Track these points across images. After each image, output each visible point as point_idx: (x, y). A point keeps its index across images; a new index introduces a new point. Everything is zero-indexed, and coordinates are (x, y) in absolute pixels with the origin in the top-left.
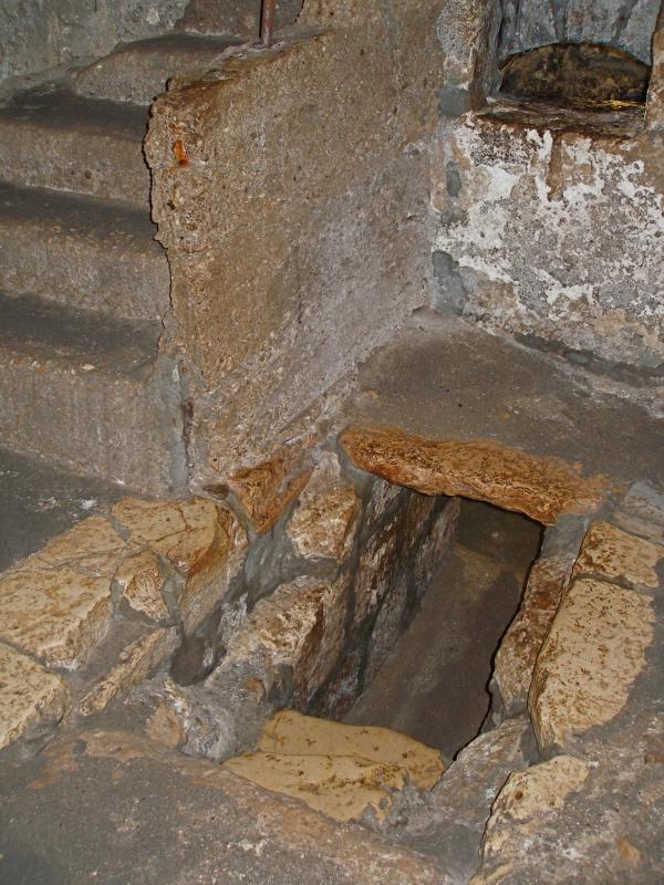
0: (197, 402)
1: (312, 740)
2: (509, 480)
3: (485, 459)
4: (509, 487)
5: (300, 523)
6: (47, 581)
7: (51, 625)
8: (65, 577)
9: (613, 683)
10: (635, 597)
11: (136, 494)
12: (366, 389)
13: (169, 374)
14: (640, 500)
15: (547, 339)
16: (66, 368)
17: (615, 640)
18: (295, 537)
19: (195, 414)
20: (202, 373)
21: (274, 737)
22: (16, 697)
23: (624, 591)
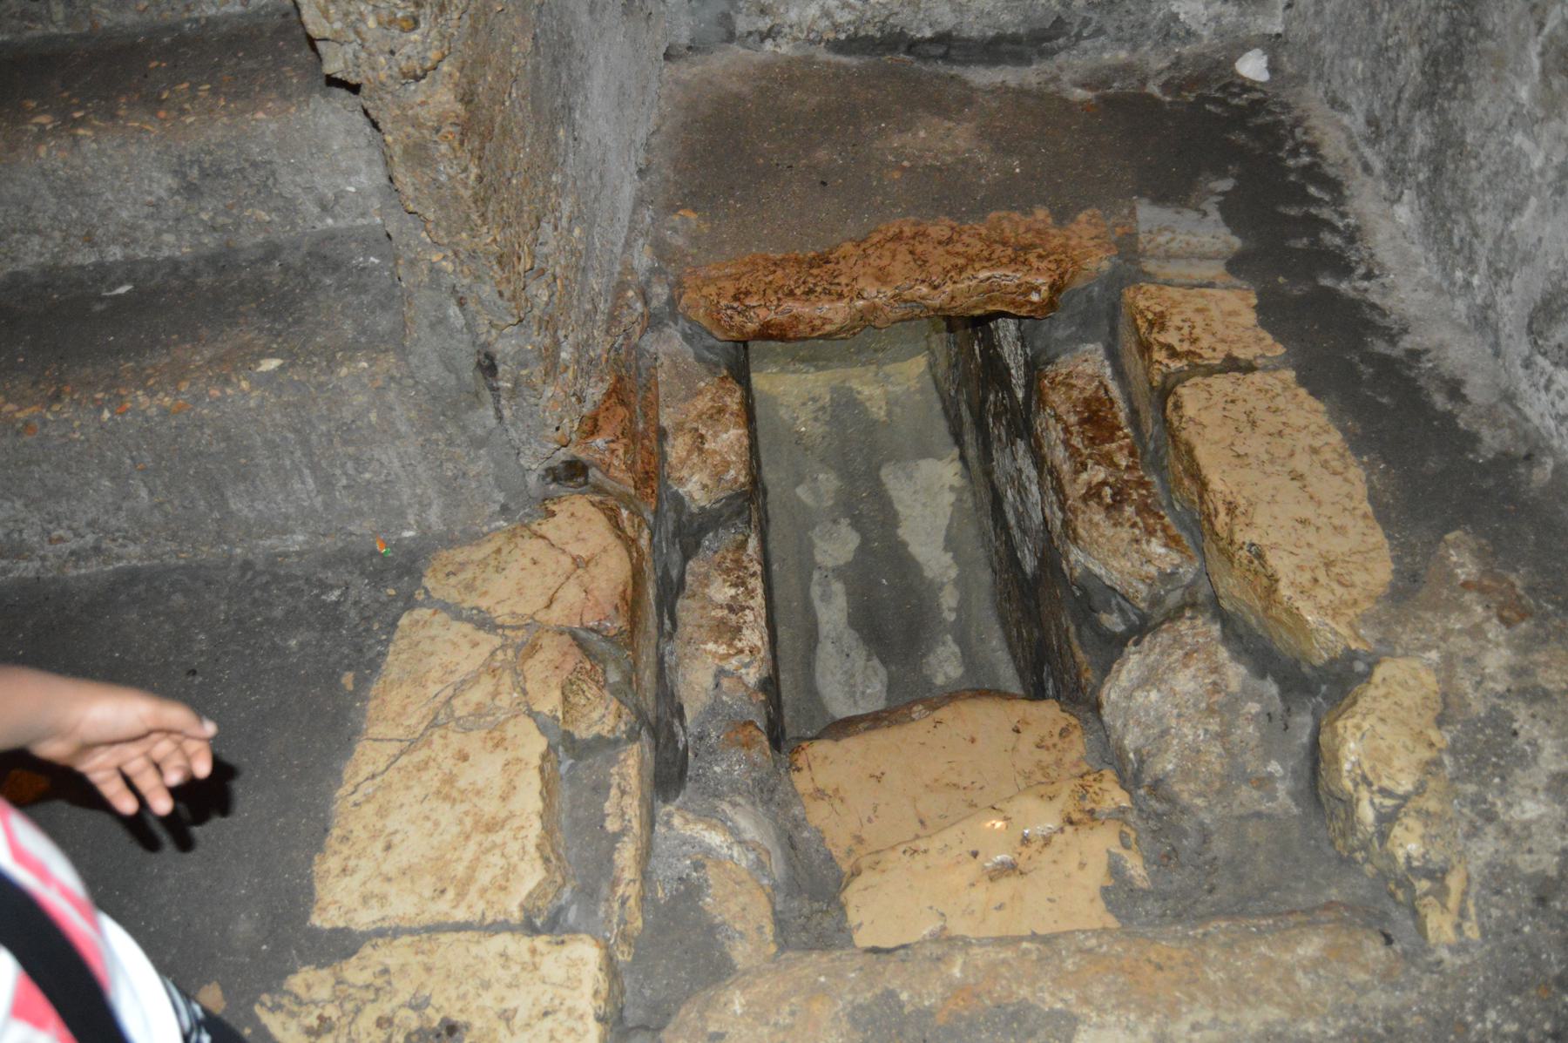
0: (499, 346)
1: (878, 774)
2: (970, 272)
3: (911, 252)
4: (974, 282)
5: (683, 462)
6: (425, 776)
7: (498, 852)
8: (449, 753)
9: (1346, 520)
10: (1270, 380)
11: (450, 542)
12: (672, 208)
13: (443, 320)
14: (1160, 231)
15: (878, 35)
16: (227, 381)
17: (1297, 456)
18: (683, 485)
19: (501, 369)
20: (501, 294)
21: (820, 794)
22: (548, 1023)
23: (1250, 377)
